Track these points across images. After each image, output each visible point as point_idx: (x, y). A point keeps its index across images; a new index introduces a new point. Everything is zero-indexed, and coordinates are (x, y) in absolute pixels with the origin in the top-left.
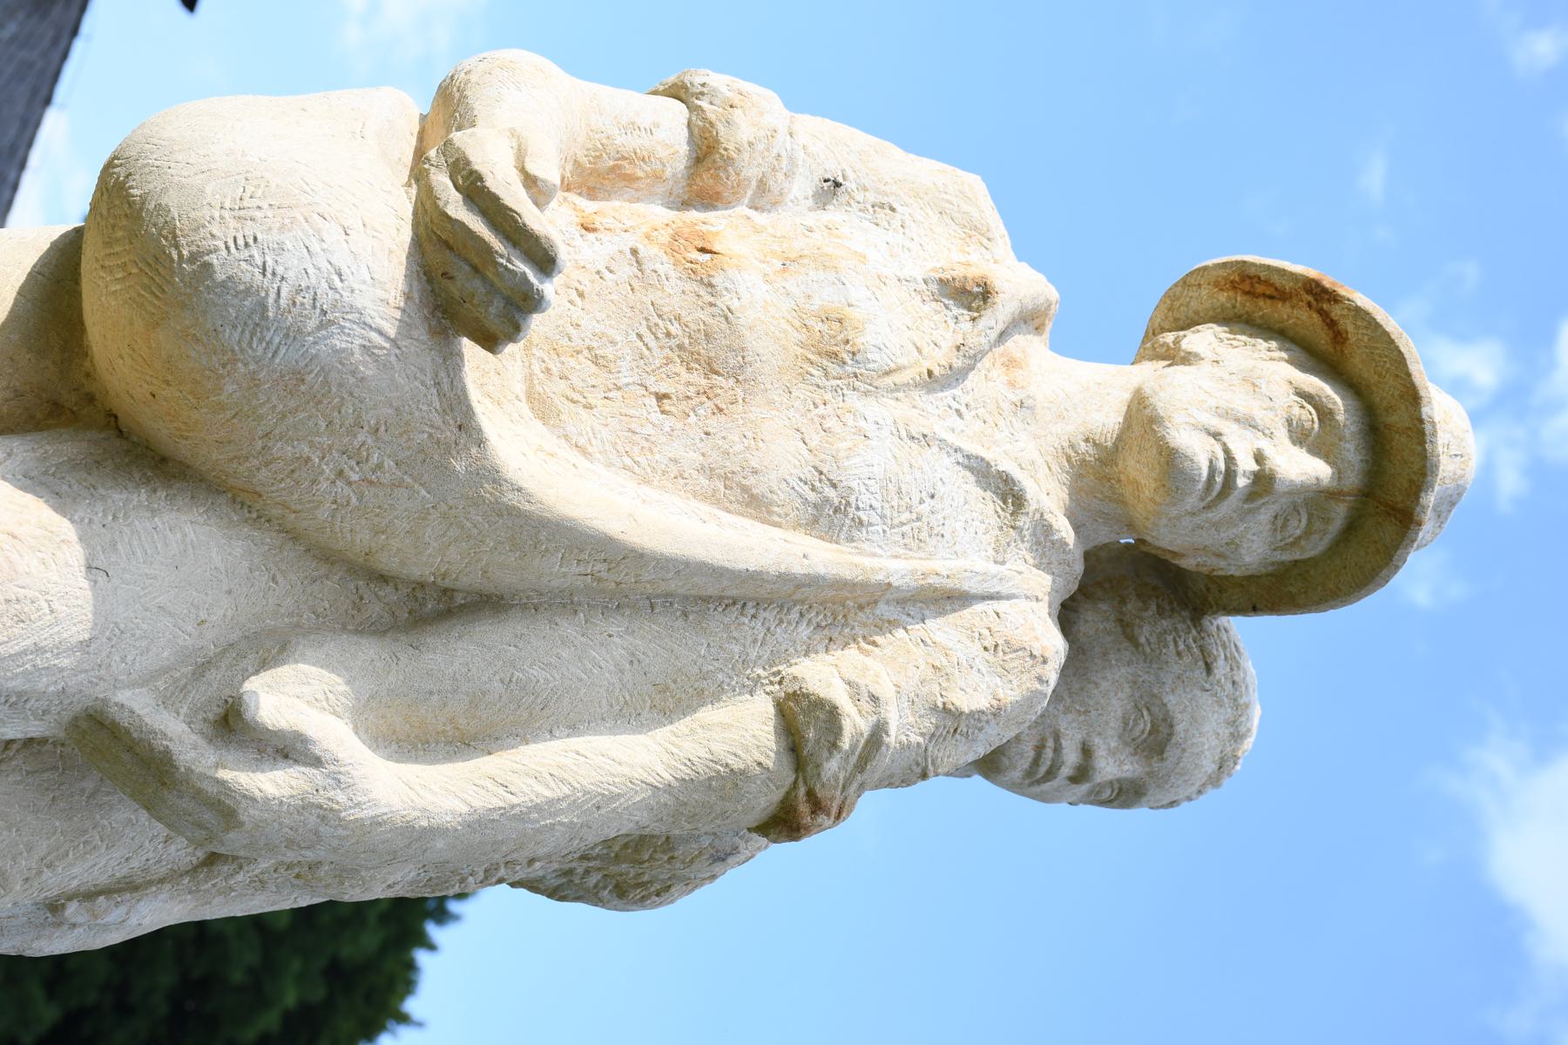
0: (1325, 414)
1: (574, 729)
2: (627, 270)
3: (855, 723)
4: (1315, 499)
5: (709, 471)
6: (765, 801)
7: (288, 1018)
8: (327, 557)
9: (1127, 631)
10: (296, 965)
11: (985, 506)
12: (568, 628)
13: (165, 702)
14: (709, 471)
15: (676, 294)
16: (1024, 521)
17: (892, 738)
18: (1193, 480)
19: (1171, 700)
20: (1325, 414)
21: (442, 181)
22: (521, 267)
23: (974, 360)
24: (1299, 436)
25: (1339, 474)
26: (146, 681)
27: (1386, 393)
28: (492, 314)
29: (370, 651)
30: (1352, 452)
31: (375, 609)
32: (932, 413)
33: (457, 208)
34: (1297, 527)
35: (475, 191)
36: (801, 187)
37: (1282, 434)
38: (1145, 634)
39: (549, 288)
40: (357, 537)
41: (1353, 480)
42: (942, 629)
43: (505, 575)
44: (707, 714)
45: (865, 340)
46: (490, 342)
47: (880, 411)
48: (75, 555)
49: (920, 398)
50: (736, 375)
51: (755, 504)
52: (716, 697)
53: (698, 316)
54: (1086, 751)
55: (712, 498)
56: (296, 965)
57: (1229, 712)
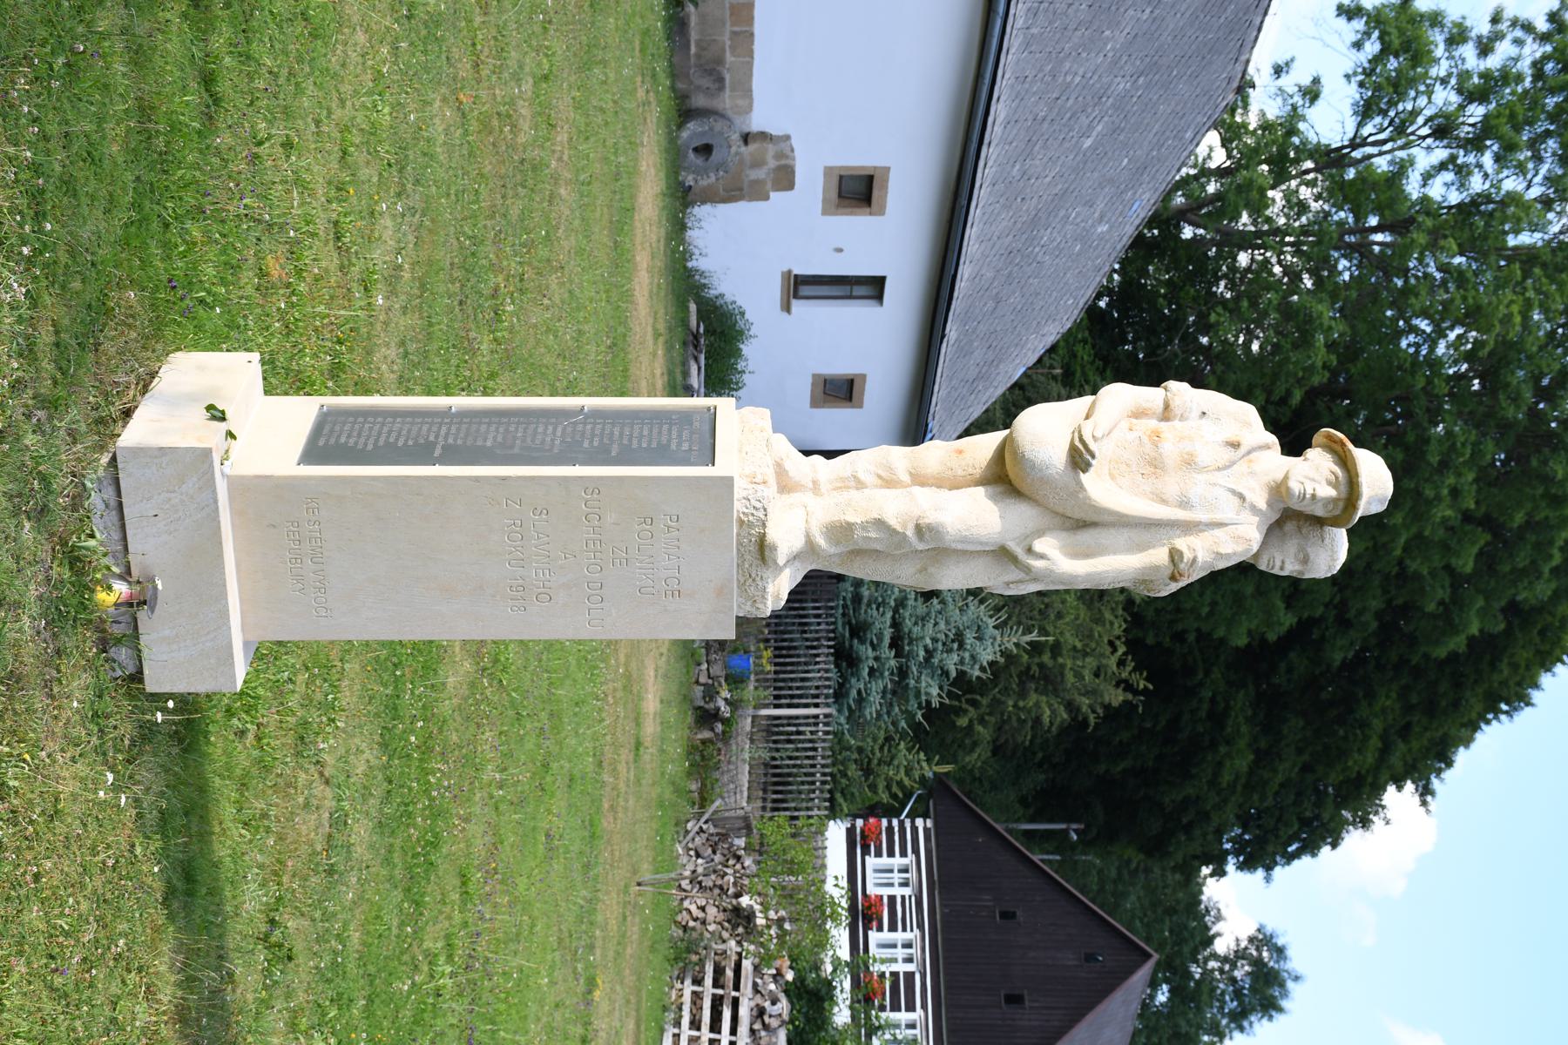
0: (1337, 478)
1: (1115, 553)
2: (1137, 442)
3: (1188, 555)
4: (1334, 501)
5: (1152, 493)
6: (1168, 572)
7: (1472, 640)
8: (1057, 513)
9: (1299, 529)
10: (1480, 602)
11: (1236, 500)
12: (1112, 531)
13: (1018, 544)
14: (1152, 493)
15: (1148, 448)
16: (1246, 505)
17: (1200, 559)
18: (1293, 495)
19: (1309, 550)
20: (1337, 478)
21: (1076, 435)
22: (1089, 457)
23: (1234, 463)
24: (1329, 483)
25: (1339, 494)
26: (1014, 539)
27: (1353, 474)
28: (1083, 466)
29: (1064, 534)
30: (1343, 488)
31: (1068, 524)
32: (1220, 478)
33: (1077, 443)
34: (1331, 507)
35: (1082, 440)
36: (1196, 413)
37: (1324, 482)
38: (1304, 531)
39: (1094, 462)
40: (1061, 510)
41: (1344, 495)
42: (1218, 532)
43: (1095, 518)
44: (1151, 551)
45: (1198, 460)
46: (1084, 472)
47: (1201, 477)
48: (998, 514)
49: (1217, 473)
50: (1162, 469)
51: (1164, 501)
52: (1154, 547)
53: (1153, 454)
54: (1283, 562)
55: (1153, 500)
56: (1480, 602)
57: (1329, 553)
